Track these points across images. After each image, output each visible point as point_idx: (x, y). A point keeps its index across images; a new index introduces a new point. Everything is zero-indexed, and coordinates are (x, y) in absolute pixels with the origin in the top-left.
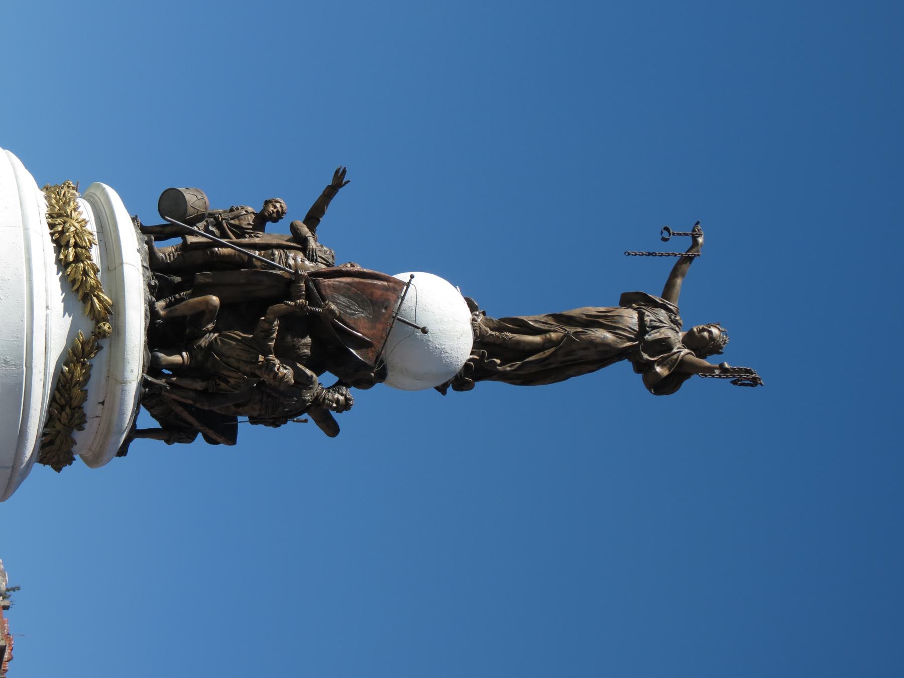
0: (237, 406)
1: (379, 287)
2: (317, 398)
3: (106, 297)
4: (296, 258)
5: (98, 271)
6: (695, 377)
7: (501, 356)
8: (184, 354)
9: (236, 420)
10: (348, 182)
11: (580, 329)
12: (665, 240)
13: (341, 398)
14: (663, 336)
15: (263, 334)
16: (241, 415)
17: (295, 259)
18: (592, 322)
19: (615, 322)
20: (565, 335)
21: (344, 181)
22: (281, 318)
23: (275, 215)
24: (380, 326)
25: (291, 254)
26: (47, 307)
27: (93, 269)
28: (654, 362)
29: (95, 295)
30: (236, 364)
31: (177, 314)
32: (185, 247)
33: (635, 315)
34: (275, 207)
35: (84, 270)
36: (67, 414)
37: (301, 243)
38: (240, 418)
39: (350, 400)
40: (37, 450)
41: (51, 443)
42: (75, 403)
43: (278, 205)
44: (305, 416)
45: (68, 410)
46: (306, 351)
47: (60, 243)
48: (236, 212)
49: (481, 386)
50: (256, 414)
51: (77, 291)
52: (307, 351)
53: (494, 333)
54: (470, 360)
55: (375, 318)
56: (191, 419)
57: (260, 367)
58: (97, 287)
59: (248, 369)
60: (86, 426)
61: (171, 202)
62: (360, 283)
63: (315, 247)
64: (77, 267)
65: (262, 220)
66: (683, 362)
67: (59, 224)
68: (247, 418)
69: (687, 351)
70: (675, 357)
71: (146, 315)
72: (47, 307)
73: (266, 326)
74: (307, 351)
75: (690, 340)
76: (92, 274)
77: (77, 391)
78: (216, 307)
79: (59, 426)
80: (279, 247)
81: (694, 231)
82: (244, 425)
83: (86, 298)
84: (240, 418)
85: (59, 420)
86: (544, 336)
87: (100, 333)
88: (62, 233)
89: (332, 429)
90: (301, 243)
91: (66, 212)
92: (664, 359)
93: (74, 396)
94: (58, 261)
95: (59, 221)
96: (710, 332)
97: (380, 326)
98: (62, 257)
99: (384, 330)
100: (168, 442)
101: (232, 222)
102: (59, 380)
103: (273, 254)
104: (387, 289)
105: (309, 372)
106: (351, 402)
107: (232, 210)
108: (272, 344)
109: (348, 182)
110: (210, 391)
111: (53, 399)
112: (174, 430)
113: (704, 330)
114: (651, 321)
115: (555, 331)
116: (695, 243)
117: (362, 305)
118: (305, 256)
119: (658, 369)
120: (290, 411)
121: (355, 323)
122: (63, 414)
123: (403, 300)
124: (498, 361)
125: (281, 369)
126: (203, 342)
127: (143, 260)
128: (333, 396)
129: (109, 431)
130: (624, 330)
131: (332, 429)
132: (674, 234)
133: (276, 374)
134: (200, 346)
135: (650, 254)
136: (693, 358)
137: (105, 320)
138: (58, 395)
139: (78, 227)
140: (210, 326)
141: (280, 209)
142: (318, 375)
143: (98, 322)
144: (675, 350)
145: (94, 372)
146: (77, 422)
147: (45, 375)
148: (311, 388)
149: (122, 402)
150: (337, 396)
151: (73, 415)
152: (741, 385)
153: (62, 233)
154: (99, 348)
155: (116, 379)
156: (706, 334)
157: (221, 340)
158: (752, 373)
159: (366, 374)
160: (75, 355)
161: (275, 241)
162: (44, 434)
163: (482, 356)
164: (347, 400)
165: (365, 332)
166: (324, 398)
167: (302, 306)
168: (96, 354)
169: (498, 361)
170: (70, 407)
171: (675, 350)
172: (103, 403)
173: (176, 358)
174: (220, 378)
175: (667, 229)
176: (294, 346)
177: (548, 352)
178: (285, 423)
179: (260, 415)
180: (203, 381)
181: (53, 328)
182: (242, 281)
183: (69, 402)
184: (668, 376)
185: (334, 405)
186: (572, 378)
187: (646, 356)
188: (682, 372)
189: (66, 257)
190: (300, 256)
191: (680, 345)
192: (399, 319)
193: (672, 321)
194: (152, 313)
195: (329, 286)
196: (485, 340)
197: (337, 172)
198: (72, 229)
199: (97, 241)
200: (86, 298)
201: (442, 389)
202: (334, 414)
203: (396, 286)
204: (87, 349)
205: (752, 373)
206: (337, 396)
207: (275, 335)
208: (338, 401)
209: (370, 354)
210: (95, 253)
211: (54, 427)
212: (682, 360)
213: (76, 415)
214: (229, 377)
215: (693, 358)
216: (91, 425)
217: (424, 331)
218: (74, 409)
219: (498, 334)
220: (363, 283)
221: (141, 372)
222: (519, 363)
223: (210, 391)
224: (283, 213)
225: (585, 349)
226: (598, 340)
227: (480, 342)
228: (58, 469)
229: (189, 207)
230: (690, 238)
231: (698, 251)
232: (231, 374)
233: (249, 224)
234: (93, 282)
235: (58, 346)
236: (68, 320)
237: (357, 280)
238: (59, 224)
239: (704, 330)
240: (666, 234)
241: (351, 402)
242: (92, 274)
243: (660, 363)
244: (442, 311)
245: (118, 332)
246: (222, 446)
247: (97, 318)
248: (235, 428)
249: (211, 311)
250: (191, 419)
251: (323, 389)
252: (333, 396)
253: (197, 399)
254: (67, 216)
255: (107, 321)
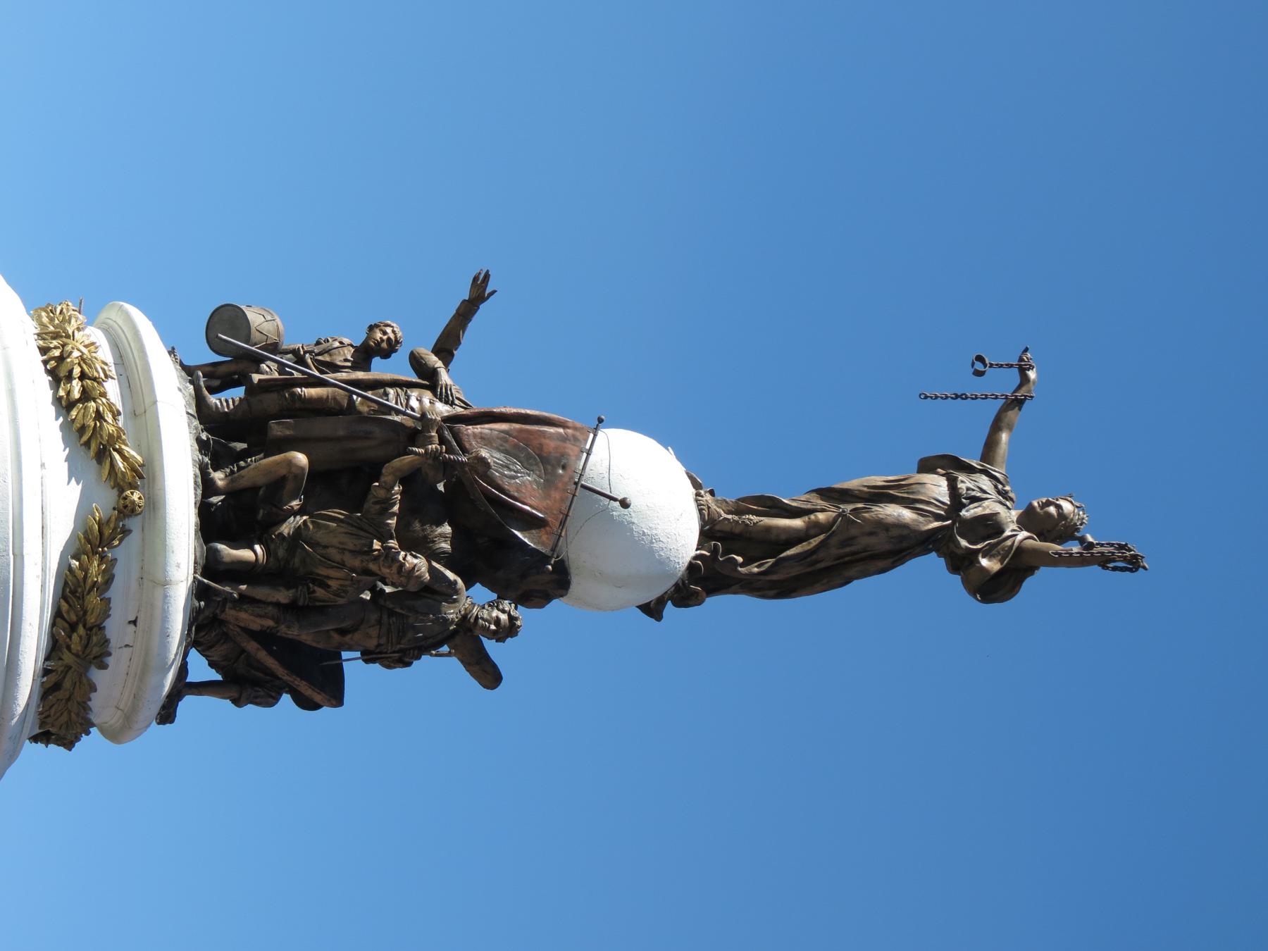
0: (343, 632)
1: (551, 436)
2: (465, 618)
3: (133, 453)
4: (419, 401)
5: (119, 413)
6: (1043, 573)
7: (746, 556)
8: (257, 547)
9: (340, 657)
10: (494, 292)
11: (860, 505)
12: (979, 374)
13: (504, 617)
14: (987, 512)
15: (378, 507)
16: (350, 649)
17: (420, 401)
18: (879, 495)
19: (913, 493)
20: (839, 515)
21: (488, 291)
22: (403, 481)
23: (384, 345)
24: (556, 495)
25: (414, 394)
26: (43, 465)
27: (112, 411)
28: (978, 551)
29: (115, 450)
30: (338, 557)
31: (244, 483)
32: (252, 390)
33: (944, 483)
34: (385, 333)
35: (98, 412)
36: (81, 637)
37: (429, 379)
38: (345, 655)
39: (516, 619)
40: (36, 698)
41: (56, 687)
42: (91, 619)
43: (389, 330)
44: (445, 649)
45: (81, 630)
46: (443, 545)
47: (58, 373)
48: (324, 346)
49: (718, 604)
50: (372, 644)
51: (87, 444)
52: (446, 546)
53: (730, 517)
54: (696, 557)
55: (549, 483)
56: (271, 663)
57: (376, 558)
58: (119, 437)
59: (357, 563)
60: (110, 661)
61: (227, 321)
62: (521, 431)
63: (449, 382)
64: (86, 408)
65: (365, 354)
66: (1021, 550)
67: (56, 348)
68: (358, 654)
69: (1025, 534)
70: (1009, 543)
71: (196, 483)
72: (43, 465)
73: (382, 494)
74: (446, 546)
75: (1029, 519)
76: (109, 417)
77: (93, 600)
78: (302, 469)
79: (68, 658)
80: (395, 384)
81: (1021, 360)
82: (355, 670)
83: (102, 455)
84: (345, 655)
85: (69, 648)
86: (806, 518)
87: (126, 507)
88: (61, 359)
89: (489, 675)
90: (429, 379)
91: (65, 331)
92: (992, 546)
93: (90, 607)
94: (57, 401)
95: (55, 343)
96: (1059, 507)
97: (556, 495)
98: (62, 393)
99: (562, 500)
100: (237, 702)
101: (320, 358)
102: (66, 583)
103: (386, 394)
104: (564, 439)
105: (451, 575)
106: (518, 623)
107: (318, 343)
108: (392, 522)
109: (494, 292)
110: (301, 603)
111: (57, 615)
112: (244, 683)
113: (1049, 503)
114: (968, 489)
115: (823, 511)
116: (1025, 380)
117: (528, 463)
118: (435, 395)
119: (984, 562)
120: (425, 638)
121: (518, 491)
122: (75, 636)
123: (588, 454)
124: (740, 559)
125: (409, 558)
126: (287, 528)
127: (188, 404)
128: (489, 614)
129: (148, 666)
130: (928, 503)
131: (489, 675)
132: (991, 365)
133: (402, 565)
134: (281, 534)
135: (957, 397)
136: (1036, 543)
137: (133, 487)
138: (65, 606)
139: (85, 351)
140: (295, 503)
141: (392, 336)
142: (468, 585)
143: (122, 491)
144: (1008, 533)
145: (118, 571)
146: (96, 650)
147: (44, 570)
148: (455, 601)
149: (166, 635)
150: (495, 613)
151: (89, 638)
152: (1115, 569)
153: (61, 359)
154: (126, 532)
155: (153, 580)
156: (1052, 509)
157: (313, 522)
158: (1130, 550)
159: (539, 580)
160: (89, 541)
161: (388, 376)
162: (46, 672)
163: (714, 551)
164: (512, 619)
165: (533, 501)
166: (477, 618)
167: (435, 455)
168: (121, 540)
169: (740, 559)
170: (84, 626)
171: (1008, 533)
172: (134, 622)
173: (246, 554)
174: (314, 581)
175: (980, 359)
176: (426, 537)
177: (814, 542)
178: (418, 658)
179: (379, 645)
180: (288, 588)
181: (54, 505)
182: (341, 433)
183: (82, 618)
184: (1000, 573)
185: (493, 627)
186: (855, 582)
187: (964, 543)
188: (1020, 567)
189: (68, 393)
190: (427, 397)
191: (1014, 526)
192: (583, 486)
193: (999, 493)
194: (207, 487)
195: (475, 435)
196: (717, 527)
197: (476, 279)
198: (76, 354)
199: (113, 373)
200: (102, 455)
201: (653, 610)
202: (490, 646)
203: (578, 434)
204: (107, 532)
205: (1130, 550)
206: (495, 613)
207: (396, 508)
208: (497, 621)
209: (544, 538)
210: (112, 389)
211: (60, 659)
212: (1018, 548)
213: (95, 639)
214: (328, 577)
215: (1036, 543)
216: (118, 660)
217: (624, 504)
218: (91, 629)
219: (736, 518)
220: (528, 431)
221: (192, 571)
222: (771, 561)
223: (301, 603)
224: (397, 342)
225: (871, 534)
226: (890, 520)
227: (710, 531)
228: (69, 745)
229: (253, 330)
230: (1015, 371)
231: (1029, 391)
232: (332, 573)
233: (346, 360)
234: (111, 429)
235: (62, 529)
236: (75, 490)
237: (517, 426)
238: (56, 348)
239: (1049, 503)
240: (979, 366)
241: (518, 623)
242: (109, 417)
243: (987, 553)
244: (651, 489)
245: (154, 505)
246: (326, 711)
247: (120, 484)
248: (340, 669)
249: (296, 476)
250: (271, 663)
251: (473, 604)
252: (489, 614)
253: (278, 633)
254: (68, 336)
255: (136, 488)
